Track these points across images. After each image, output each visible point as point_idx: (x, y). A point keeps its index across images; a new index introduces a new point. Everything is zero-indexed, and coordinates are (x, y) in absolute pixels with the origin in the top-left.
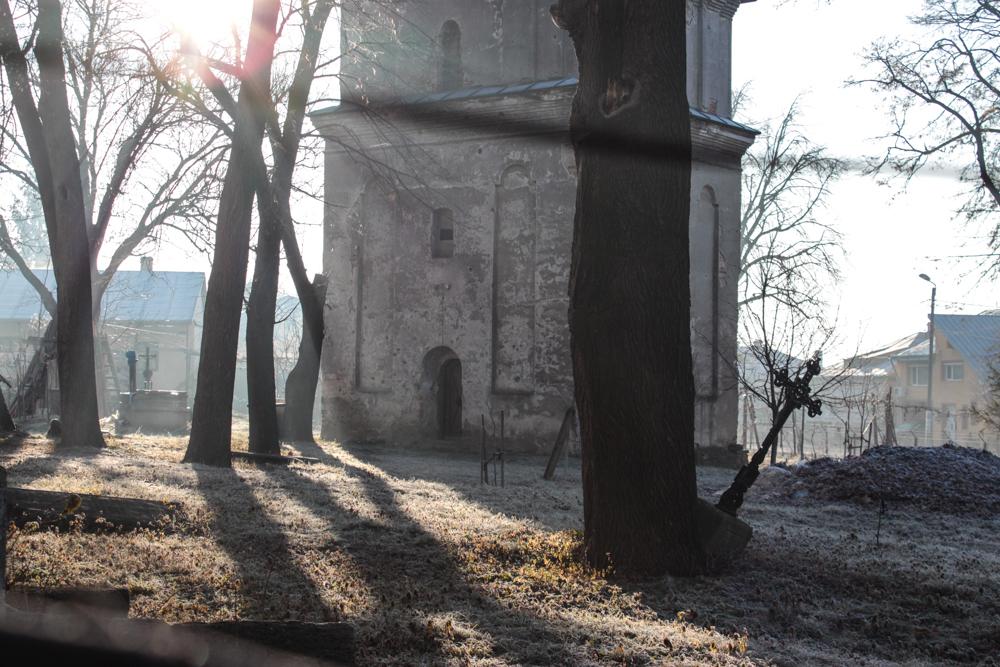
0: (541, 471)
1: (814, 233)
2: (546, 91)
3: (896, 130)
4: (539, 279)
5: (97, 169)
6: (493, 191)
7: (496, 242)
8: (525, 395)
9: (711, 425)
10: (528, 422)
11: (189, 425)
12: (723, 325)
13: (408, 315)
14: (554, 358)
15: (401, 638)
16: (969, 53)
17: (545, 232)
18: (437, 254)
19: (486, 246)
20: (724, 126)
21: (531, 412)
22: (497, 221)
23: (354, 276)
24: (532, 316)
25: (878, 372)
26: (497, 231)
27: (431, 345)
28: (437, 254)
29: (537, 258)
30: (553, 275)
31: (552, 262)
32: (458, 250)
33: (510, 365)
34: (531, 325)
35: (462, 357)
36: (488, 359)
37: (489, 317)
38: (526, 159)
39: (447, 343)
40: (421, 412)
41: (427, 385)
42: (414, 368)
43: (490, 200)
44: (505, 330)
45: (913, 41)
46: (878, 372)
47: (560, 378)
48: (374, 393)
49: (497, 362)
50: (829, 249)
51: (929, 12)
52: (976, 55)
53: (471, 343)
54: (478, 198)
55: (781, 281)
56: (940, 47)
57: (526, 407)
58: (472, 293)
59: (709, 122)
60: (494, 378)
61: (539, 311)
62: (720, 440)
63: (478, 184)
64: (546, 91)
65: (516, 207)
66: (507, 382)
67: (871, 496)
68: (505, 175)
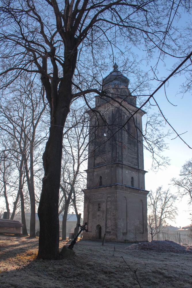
0: (101, 244)
1: (173, 208)
2: (112, 186)
3: (179, 191)
4: (112, 214)
5: (64, 199)
6: (106, 200)
7: (106, 208)
8: (110, 232)
9: (143, 238)
10: (110, 237)
11: (62, 236)
12: (145, 222)
13: (94, 220)
14: (114, 226)
15: (82, 272)
16: (189, 180)
17: (113, 207)
18: (98, 210)
19: (105, 209)
20: (143, 191)
21: (111, 235)
22: (106, 205)
23: (87, 214)
24: (111, 220)
25: (187, 229)
26: (106, 207)
27: (97, 224)
28: (98, 210)
29: (112, 211)
30: (114, 213)
31: (114, 211)
32: (101, 210)
33: (108, 227)
34: (111, 221)
35: (101, 226)
36: (105, 227)
37: (105, 220)
38: (110, 196)
39: (99, 224)
40: (96, 235)
41: (97, 230)
42: (95, 228)
43: (105, 202)
44: (107, 222)
45: (179, 178)
46: (187, 229)
47: (115, 229)
48: (90, 232)
49: (106, 227)
50: (176, 210)
51: (181, 174)
52: (190, 180)
53: (103, 225)
54: (104, 202)
55: (168, 215)
56: (185, 179)
57: (110, 234)
58: (103, 216)
59: (140, 190)
60: (106, 229)
61: (112, 219)
62: (144, 240)
63: (104, 200)
64: (112, 186)
65: (109, 203)
66: (108, 230)
67: (147, 249)
68: (108, 198)
